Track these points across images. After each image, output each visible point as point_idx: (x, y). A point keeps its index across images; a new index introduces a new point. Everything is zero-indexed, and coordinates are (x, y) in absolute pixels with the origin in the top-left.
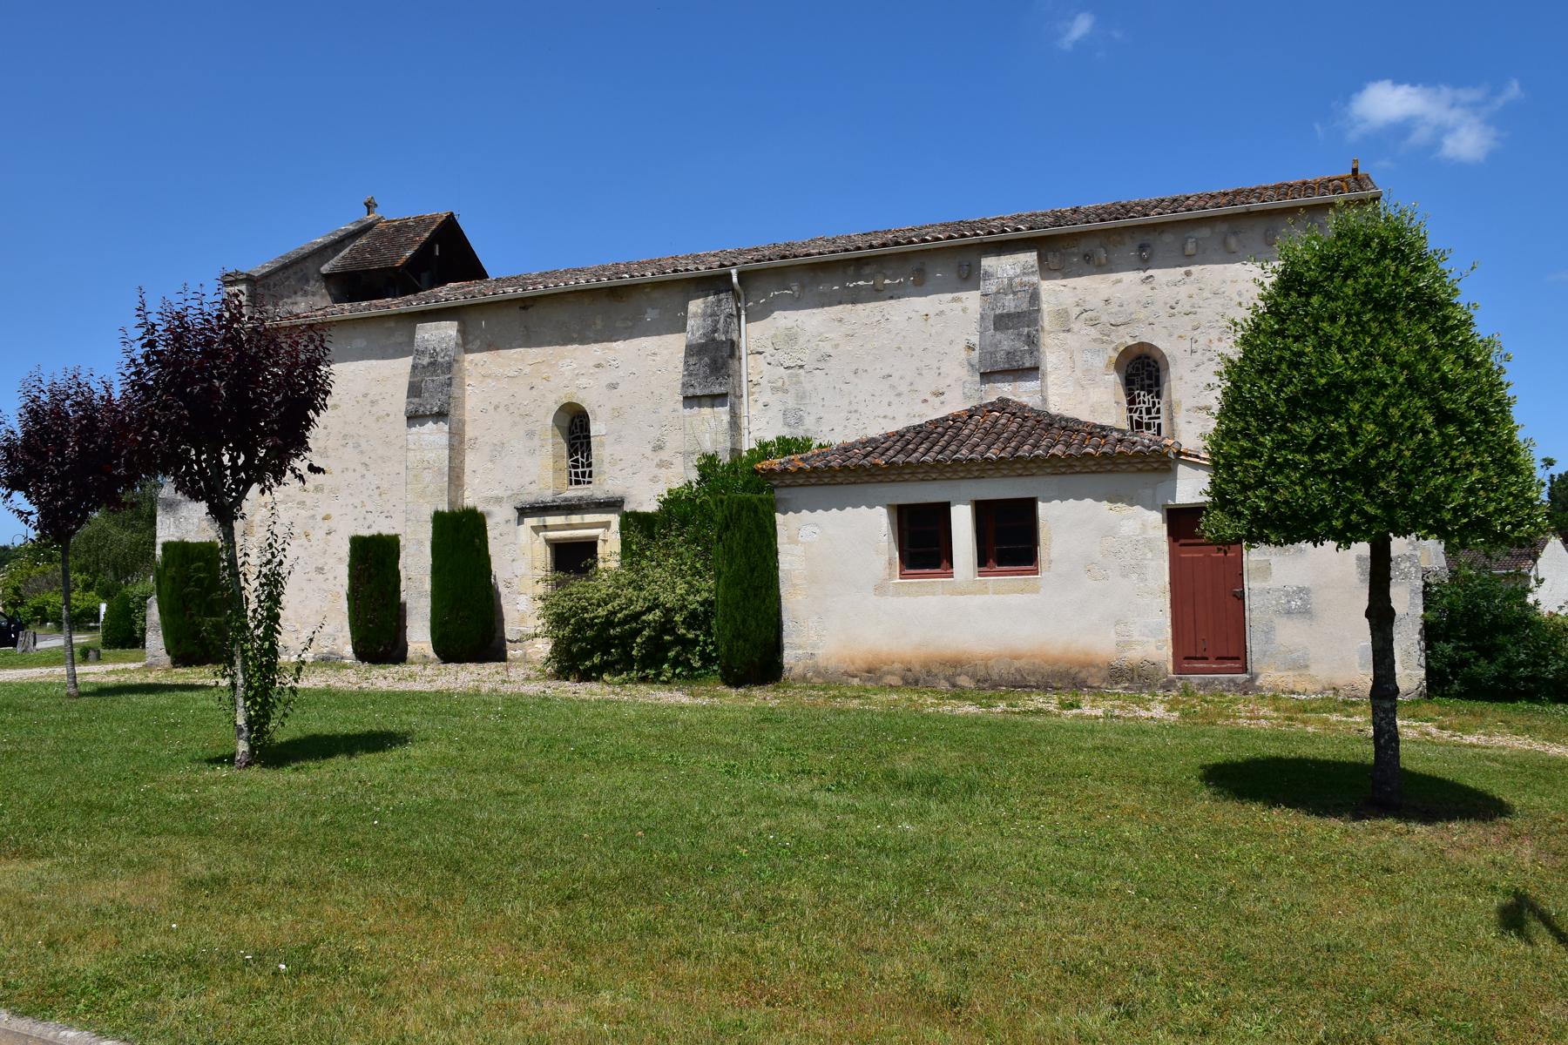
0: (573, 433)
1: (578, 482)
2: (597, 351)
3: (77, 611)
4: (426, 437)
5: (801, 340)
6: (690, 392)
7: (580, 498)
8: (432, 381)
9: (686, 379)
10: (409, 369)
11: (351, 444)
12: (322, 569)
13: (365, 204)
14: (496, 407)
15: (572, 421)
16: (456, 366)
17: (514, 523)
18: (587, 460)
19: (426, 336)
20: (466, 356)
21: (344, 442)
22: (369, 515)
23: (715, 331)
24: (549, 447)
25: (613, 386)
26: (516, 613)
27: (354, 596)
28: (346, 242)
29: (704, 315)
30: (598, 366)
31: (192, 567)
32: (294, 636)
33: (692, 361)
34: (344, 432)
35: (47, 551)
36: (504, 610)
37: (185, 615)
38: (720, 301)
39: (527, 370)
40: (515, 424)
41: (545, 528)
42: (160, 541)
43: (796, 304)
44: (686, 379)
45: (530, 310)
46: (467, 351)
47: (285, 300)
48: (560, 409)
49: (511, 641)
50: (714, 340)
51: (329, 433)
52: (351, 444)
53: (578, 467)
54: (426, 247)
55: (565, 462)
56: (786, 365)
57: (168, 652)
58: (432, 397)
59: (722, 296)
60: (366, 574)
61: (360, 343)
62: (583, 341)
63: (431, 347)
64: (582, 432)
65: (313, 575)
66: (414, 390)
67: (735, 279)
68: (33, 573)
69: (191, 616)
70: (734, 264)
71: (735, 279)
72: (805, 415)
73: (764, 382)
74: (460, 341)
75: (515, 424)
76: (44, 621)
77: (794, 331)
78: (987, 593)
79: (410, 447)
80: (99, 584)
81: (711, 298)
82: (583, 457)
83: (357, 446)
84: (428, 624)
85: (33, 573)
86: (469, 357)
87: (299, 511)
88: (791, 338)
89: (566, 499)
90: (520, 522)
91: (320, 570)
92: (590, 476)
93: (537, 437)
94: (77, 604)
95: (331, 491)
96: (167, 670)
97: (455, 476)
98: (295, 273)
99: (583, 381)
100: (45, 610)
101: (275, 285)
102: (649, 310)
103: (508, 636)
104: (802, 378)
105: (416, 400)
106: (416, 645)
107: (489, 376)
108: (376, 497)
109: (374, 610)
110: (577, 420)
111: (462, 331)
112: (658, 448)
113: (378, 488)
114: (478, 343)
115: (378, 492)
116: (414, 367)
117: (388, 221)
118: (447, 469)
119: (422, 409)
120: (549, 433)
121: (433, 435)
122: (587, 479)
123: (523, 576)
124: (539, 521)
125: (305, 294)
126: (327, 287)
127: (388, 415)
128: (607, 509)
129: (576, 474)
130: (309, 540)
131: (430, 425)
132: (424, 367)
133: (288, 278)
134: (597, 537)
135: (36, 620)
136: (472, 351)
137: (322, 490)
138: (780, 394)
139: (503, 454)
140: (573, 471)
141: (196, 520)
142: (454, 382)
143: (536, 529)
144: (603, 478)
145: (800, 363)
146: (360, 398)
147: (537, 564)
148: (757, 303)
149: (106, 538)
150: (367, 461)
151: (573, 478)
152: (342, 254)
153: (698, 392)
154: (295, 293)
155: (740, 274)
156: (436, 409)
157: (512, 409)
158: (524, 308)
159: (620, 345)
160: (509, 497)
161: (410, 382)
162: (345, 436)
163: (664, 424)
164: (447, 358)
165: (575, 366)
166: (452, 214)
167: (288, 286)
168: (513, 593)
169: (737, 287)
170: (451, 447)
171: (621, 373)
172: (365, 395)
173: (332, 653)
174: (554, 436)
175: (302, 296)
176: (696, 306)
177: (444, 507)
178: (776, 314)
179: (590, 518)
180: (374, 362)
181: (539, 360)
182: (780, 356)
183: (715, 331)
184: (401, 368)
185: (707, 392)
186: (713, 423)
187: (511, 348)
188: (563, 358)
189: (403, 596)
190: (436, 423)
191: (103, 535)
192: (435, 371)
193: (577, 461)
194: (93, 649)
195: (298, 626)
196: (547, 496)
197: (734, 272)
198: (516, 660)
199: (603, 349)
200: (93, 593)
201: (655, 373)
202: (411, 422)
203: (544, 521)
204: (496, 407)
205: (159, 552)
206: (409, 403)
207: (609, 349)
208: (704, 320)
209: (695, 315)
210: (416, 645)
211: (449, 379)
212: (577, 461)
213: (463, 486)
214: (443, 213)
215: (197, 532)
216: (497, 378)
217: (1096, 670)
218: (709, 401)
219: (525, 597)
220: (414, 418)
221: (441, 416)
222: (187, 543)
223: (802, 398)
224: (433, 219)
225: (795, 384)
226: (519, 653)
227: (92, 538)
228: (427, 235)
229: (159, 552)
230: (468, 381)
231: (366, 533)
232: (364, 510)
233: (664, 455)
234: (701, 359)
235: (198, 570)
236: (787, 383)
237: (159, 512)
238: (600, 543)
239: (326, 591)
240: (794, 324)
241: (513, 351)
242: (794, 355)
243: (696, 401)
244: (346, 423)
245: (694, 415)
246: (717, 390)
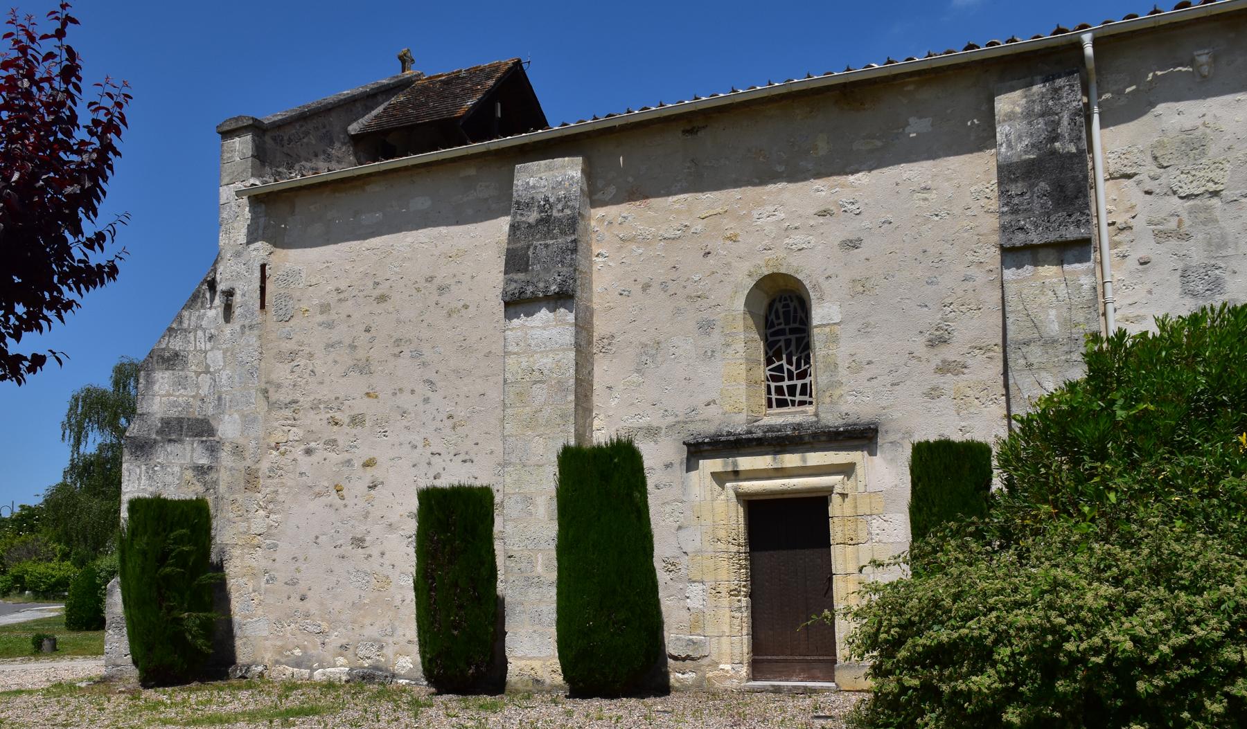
0: (772, 325)
1: (782, 403)
2: (820, 190)
3: (53, 580)
4: (538, 332)
5: (1213, 150)
6: (1019, 239)
7: (797, 427)
8: (542, 248)
9: (1007, 218)
10: (507, 228)
11: (407, 353)
12: (362, 540)
13: (400, 58)
14: (646, 287)
15: (771, 306)
16: (581, 225)
17: (679, 470)
18: (798, 367)
19: (532, 181)
20: (592, 211)
21: (397, 350)
22: (436, 459)
23: (1054, 137)
24: (740, 346)
25: (852, 244)
26: (685, 613)
27: (425, 584)
28: (380, 98)
29: (1028, 115)
30: (824, 213)
31: (172, 535)
32: (318, 641)
33: (1015, 189)
34: (396, 336)
35: (29, 521)
36: (663, 609)
37: (160, 608)
38: (1056, 91)
39: (699, 226)
40: (678, 311)
41: (736, 475)
42: (125, 498)
43: (1202, 87)
44: (1007, 218)
45: (701, 134)
46: (594, 204)
47: (303, 163)
48: (757, 285)
49: (675, 658)
50: (1054, 152)
51: (374, 338)
52: (407, 353)
53: (782, 379)
54: (490, 98)
55: (762, 372)
57: (135, 662)
58: (547, 270)
59: (1060, 82)
60: (448, 548)
61: (421, 203)
62: (795, 175)
63: (540, 197)
64: (787, 323)
65: (348, 549)
66: (515, 261)
67: (1089, 50)
68: (15, 542)
69: (170, 609)
71: (1089, 50)
72: (1227, 276)
73: (1137, 224)
74: (585, 188)
75: (678, 311)
76: (23, 590)
77: (1197, 133)
79: (510, 348)
80: (76, 554)
81: (1037, 88)
82: (790, 362)
83: (417, 355)
85: (15, 542)
86: (599, 212)
87: (326, 454)
88: (1193, 145)
89: (771, 428)
90: (691, 465)
91: (359, 542)
92: (803, 392)
93: (717, 331)
94: (54, 573)
95: (377, 423)
96: (134, 695)
98: (317, 129)
99: (797, 239)
100: (24, 578)
101: (290, 141)
102: (912, 120)
103: (671, 649)
104: (1217, 214)
105: (521, 276)
106: (522, 663)
107: (632, 239)
108: (448, 431)
109: (461, 607)
110: (779, 306)
111: (588, 173)
112: (938, 341)
113: (451, 417)
114: (612, 190)
115: (449, 423)
116: (514, 228)
117: (430, 78)
118: (572, 381)
119: (530, 289)
120: (740, 324)
122: (798, 398)
123: (699, 552)
124: (726, 464)
125: (329, 158)
126: (355, 154)
127: (466, 307)
128: (848, 443)
129: (779, 390)
130: (342, 498)
131: (543, 314)
132: (530, 226)
133: (307, 134)
134: (830, 490)
135: (17, 588)
136: (604, 204)
137: (362, 422)
138: (1173, 243)
139: (659, 359)
140: (773, 385)
141: (176, 469)
142: (580, 248)
143: (720, 478)
144: (837, 392)
146: (422, 284)
147: (722, 534)
148: (1120, 93)
149: (75, 505)
150: (431, 375)
151: (774, 396)
152: (374, 113)
153: (1035, 238)
154: (316, 155)
155: (1096, 42)
156: (554, 288)
157: (672, 287)
158: (691, 131)
159: (862, 178)
161: (507, 249)
162: (398, 342)
163: (948, 301)
164: (568, 212)
165: (783, 216)
166: (518, 64)
167: (307, 144)
168: (680, 580)
169: (1091, 65)
170: (578, 348)
171: (867, 224)
172: (430, 279)
173: (376, 668)
174: (746, 328)
175: (325, 160)
176: (1008, 103)
177: (572, 443)
178: (1161, 108)
179: (816, 458)
180: (443, 230)
181: (719, 210)
182: (1171, 177)
183: (1054, 137)
184: (504, 223)
185: (1052, 237)
186: (1062, 291)
187: (668, 194)
188: (760, 204)
189: (501, 588)
190: (553, 310)
191: (72, 502)
192: (549, 231)
193: (780, 369)
194: (47, 637)
195: (324, 625)
196: (738, 424)
197: (1087, 38)
198: (684, 689)
199: (831, 187)
200: (69, 563)
201: (927, 219)
202: (512, 310)
203: (735, 464)
204: (646, 287)
205: (124, 514)
206: (508, 282)
207: (843, 186)
208: (1030, 123)
209: (1010, 117)
210: (522, 663)
211: (575, 241)
212: (780, 369)
213: (591, 411)
214: (508, 60)
215: (179, 486)
216: (645, 241)
218: (1053, 254)
219: (701, 586)
220: (517, 304)
221: (563, 298)
222: (165, 500)
223: (1219, 247)
224: (496, 68)
225: (1204, 223)
226: (690, 677)
227: (61, 505)
228: (491, 83)
229: (124, 514)
230: (596, 249)
231: (444, 482)
232: (429, 450)
233: (948, 353)
234: (1032, 186)
235: (179, 540)
236: (1187, 222)
237: (126, 457)
238: (835, 500)
239: (366, 573)
240: (1199, 122)
241: (671, 199)
242: (1198, 174)
243: (1028, 255)
244: (399, 321)
245: (1025, 279)
246: (1072, 233)
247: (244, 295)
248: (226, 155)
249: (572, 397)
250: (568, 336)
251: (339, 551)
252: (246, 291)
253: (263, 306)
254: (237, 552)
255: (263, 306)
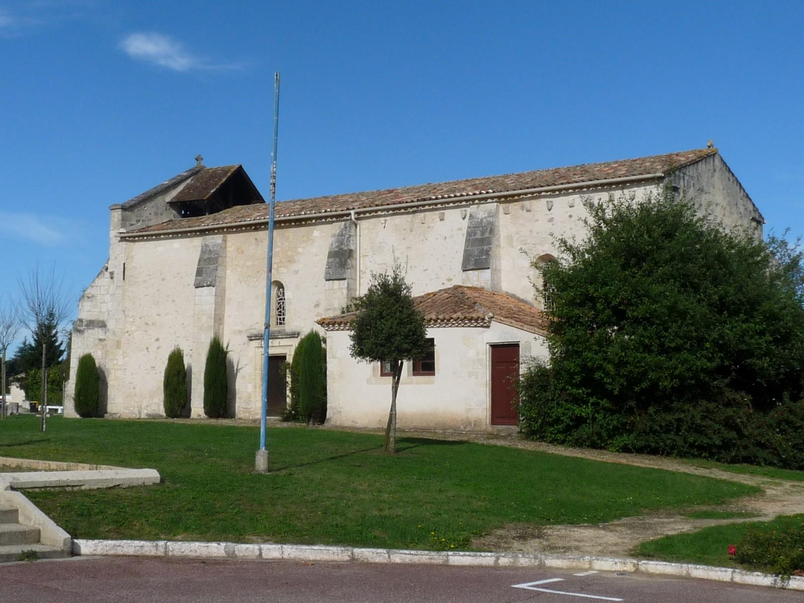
12: (154, 367)
33: (331, 260)
56: (378, 263)
70: (353, 209)
78: (412, 384)
84: (203, 401)
97: (219, 319)
121: (207, 294)
130: (148, 351)
137: (156, 325)
140: (279, 317)
141: (92, 340)
145: (384, 261)
151: (279, 321)
160: (246, 331)
161: (198, 268)
166: (241, 167)
170: (216, 303)
193: (280, 312)
210: (196, 409)
211: (217, 267)
212: (280, 312)
217: (704, 454)
228: (224, 180)
247: (117, 274)
248: (112, 219)
249: (213, 320)
250: (212, 299)
251: (147, 371)
252: (118, 272)
253: (124, 279)
254: (113, 371)
255: (124, 279)
